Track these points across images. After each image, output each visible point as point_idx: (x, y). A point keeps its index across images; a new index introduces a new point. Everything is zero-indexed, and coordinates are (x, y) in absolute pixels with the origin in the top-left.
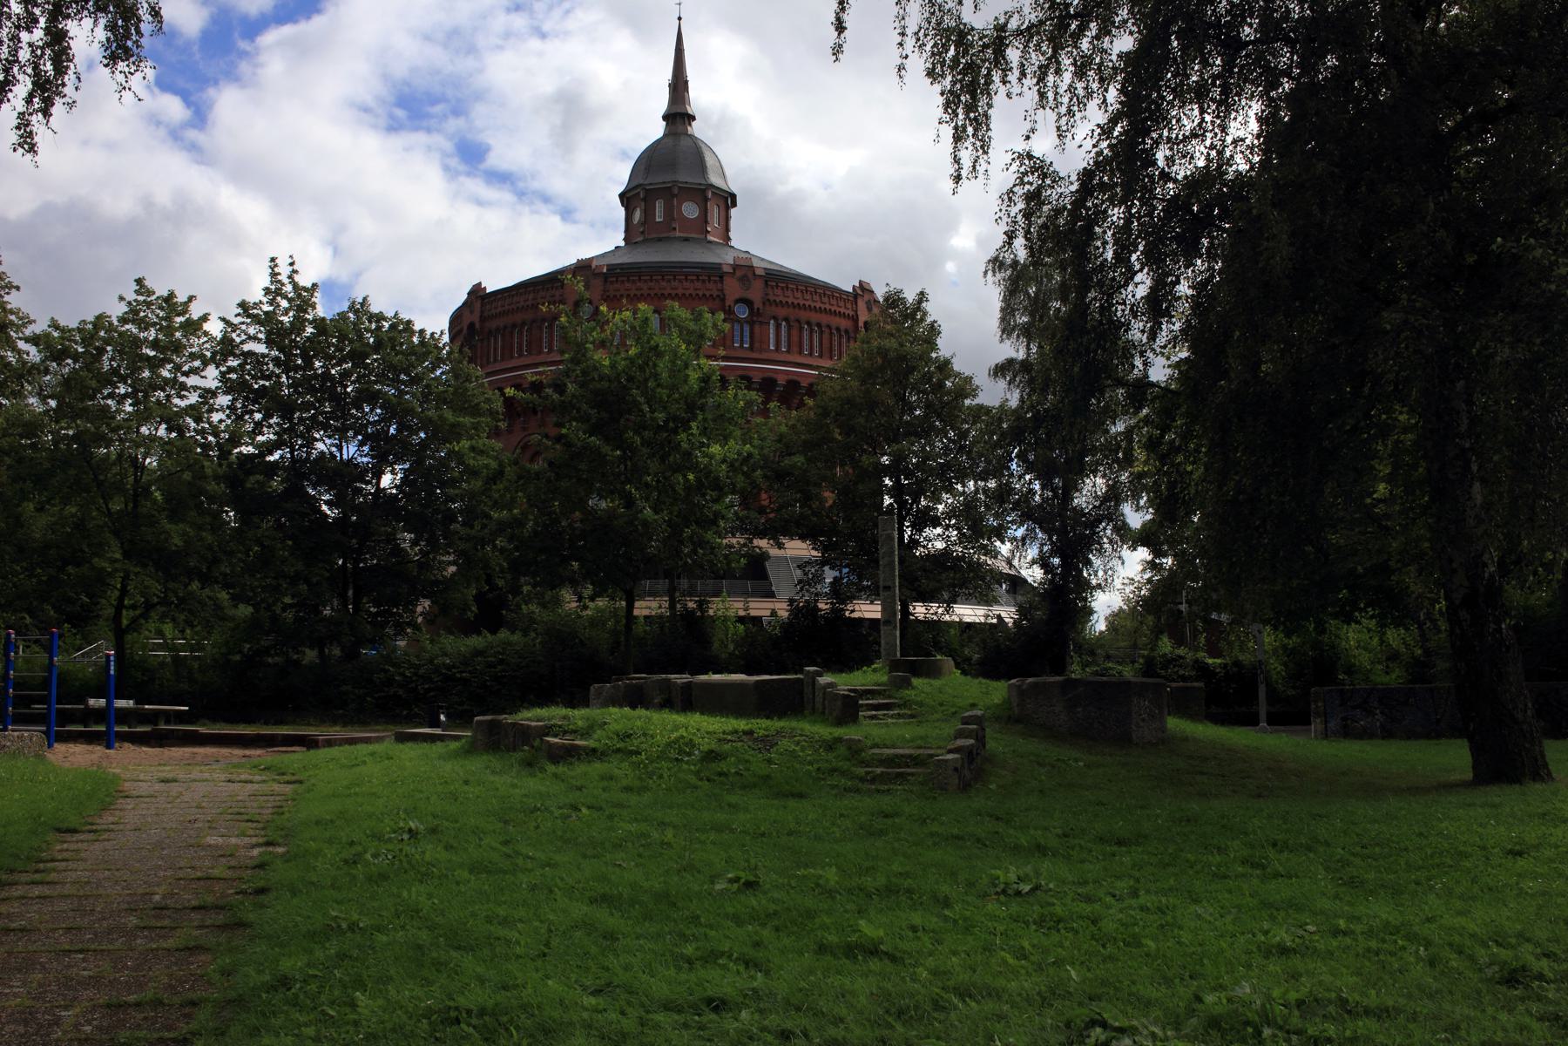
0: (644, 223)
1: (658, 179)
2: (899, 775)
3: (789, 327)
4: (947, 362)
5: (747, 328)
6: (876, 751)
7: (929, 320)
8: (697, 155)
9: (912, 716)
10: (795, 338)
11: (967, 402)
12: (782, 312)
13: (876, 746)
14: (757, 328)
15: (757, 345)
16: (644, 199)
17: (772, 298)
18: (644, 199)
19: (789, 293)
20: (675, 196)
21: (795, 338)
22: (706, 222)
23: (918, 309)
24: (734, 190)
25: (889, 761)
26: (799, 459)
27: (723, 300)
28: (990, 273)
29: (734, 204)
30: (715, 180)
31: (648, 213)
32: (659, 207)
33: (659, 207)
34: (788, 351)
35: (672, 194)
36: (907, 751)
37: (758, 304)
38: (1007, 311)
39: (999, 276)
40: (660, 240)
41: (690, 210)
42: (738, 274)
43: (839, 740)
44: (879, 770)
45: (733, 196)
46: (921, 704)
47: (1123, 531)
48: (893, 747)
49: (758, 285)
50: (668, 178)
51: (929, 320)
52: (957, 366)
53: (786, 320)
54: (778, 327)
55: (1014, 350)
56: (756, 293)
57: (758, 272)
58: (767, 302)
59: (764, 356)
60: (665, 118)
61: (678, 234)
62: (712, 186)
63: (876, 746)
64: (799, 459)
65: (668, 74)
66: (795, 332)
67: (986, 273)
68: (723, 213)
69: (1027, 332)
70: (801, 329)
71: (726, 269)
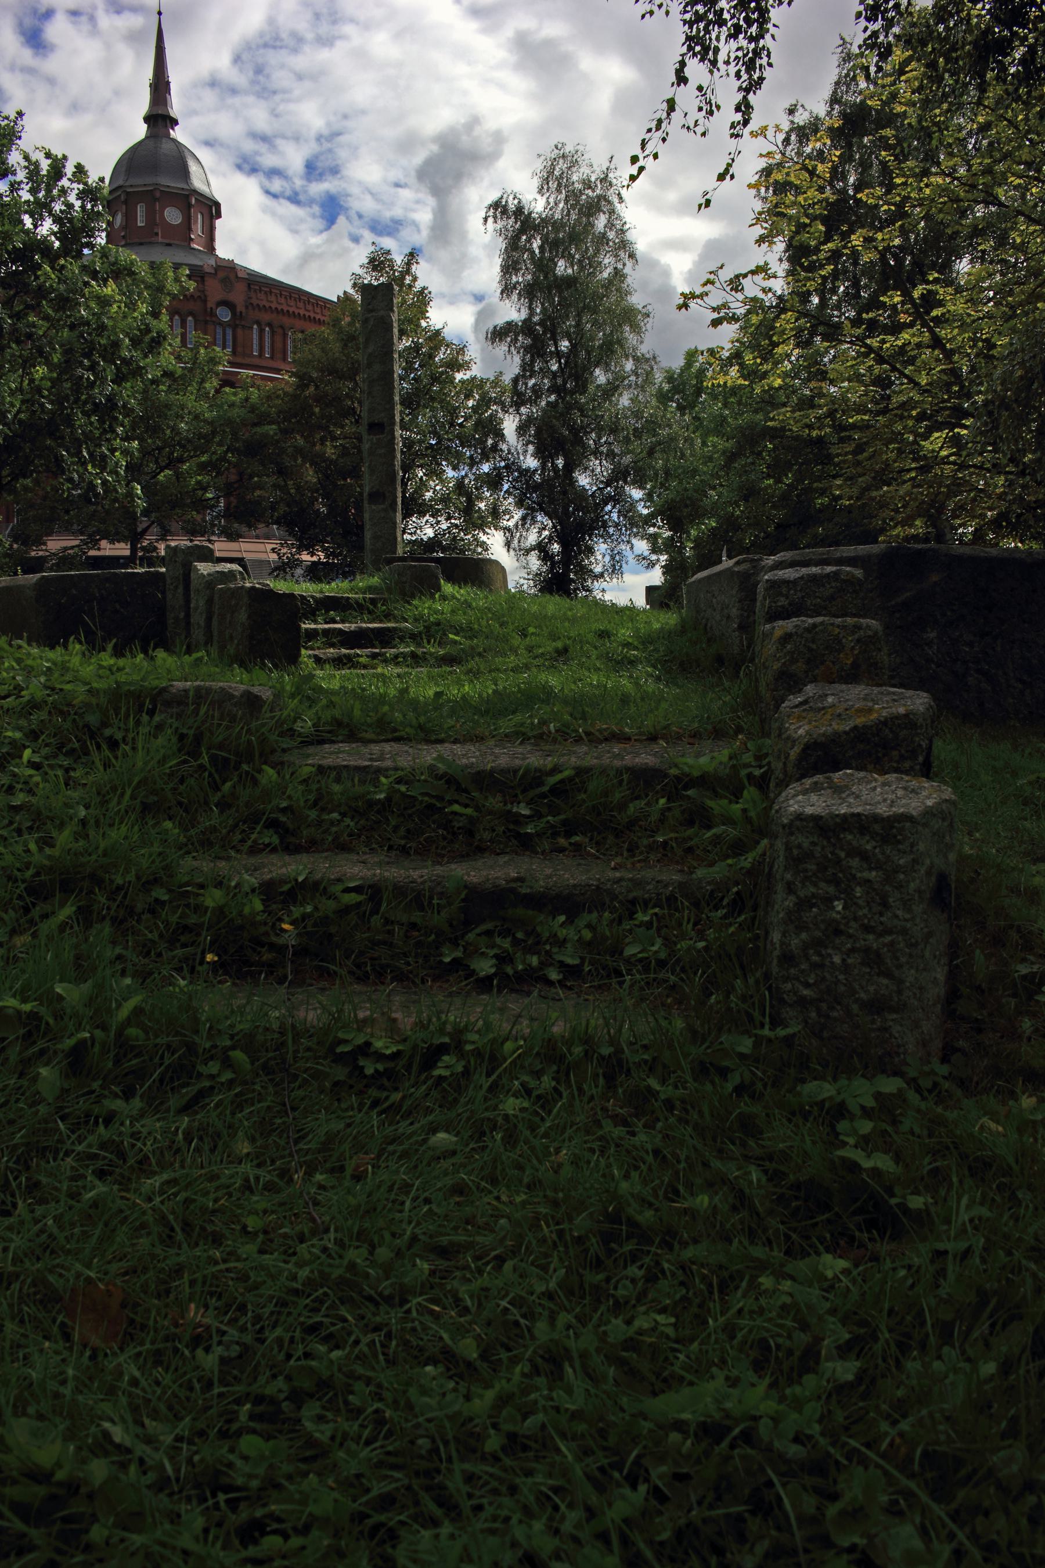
0: (125, 227)
1: (140, 182)
2: (486, 905)
3: (273, 333)
4: (438, 333)
5: (229, 332)
6: (341, 754)
7: (419, 285)
8: (179, 162)
9: (450, 660)
10: (279, 345)
11: (459, 376)
12: (266, 317)
13: (346, 730)
14: (239, 331)
15: (239, 349)
16: (126, 202)
17: (255, 301)
18: (126, 202)
19: (273, 298)
20: (156, 200)
21: (279, 345)
22: (190, 229)
23: (408, 272)
24: (218, 197)
25: (425, 817)
26: (271, 429)
27: (205, 301)
28: (490, 220)
29: (219, 215)
30: (198, 183)
31: (130, 217)
32: (140, 211)
33: (140, 211)
34: (272, 358)
35: (156, 198)
36: (502, 757)
37: (240, 308)
38: (509, 268)
39: (500, 225)
40: (141, 244)
41: (173, 216)
42: (221, 275)
43: (151, 701)
44: (356, 869)
45: (218, 205)
46: (469, 632)
47: (628, 511)
48: (428, 735)
49: (241, 287)
50: (149, 180)
51: (419, 285)
52: (447, 333)
53: (270, 325)
54: (261, 332)
55: (512, 312)
56: (238, 297)
57: (240, 275)
58: (249, 305)
59: (247, 361)
60: (147, 119)
61: (160, 240)
62: (195, 192)
63: (346, 730)
64: (271, 429)
65: (149, 73)
66: (278, 339)
67: (486, 219)
68: (207, 222)
69: (530, 292)
70: (285, 335)
71: (207, 270)
